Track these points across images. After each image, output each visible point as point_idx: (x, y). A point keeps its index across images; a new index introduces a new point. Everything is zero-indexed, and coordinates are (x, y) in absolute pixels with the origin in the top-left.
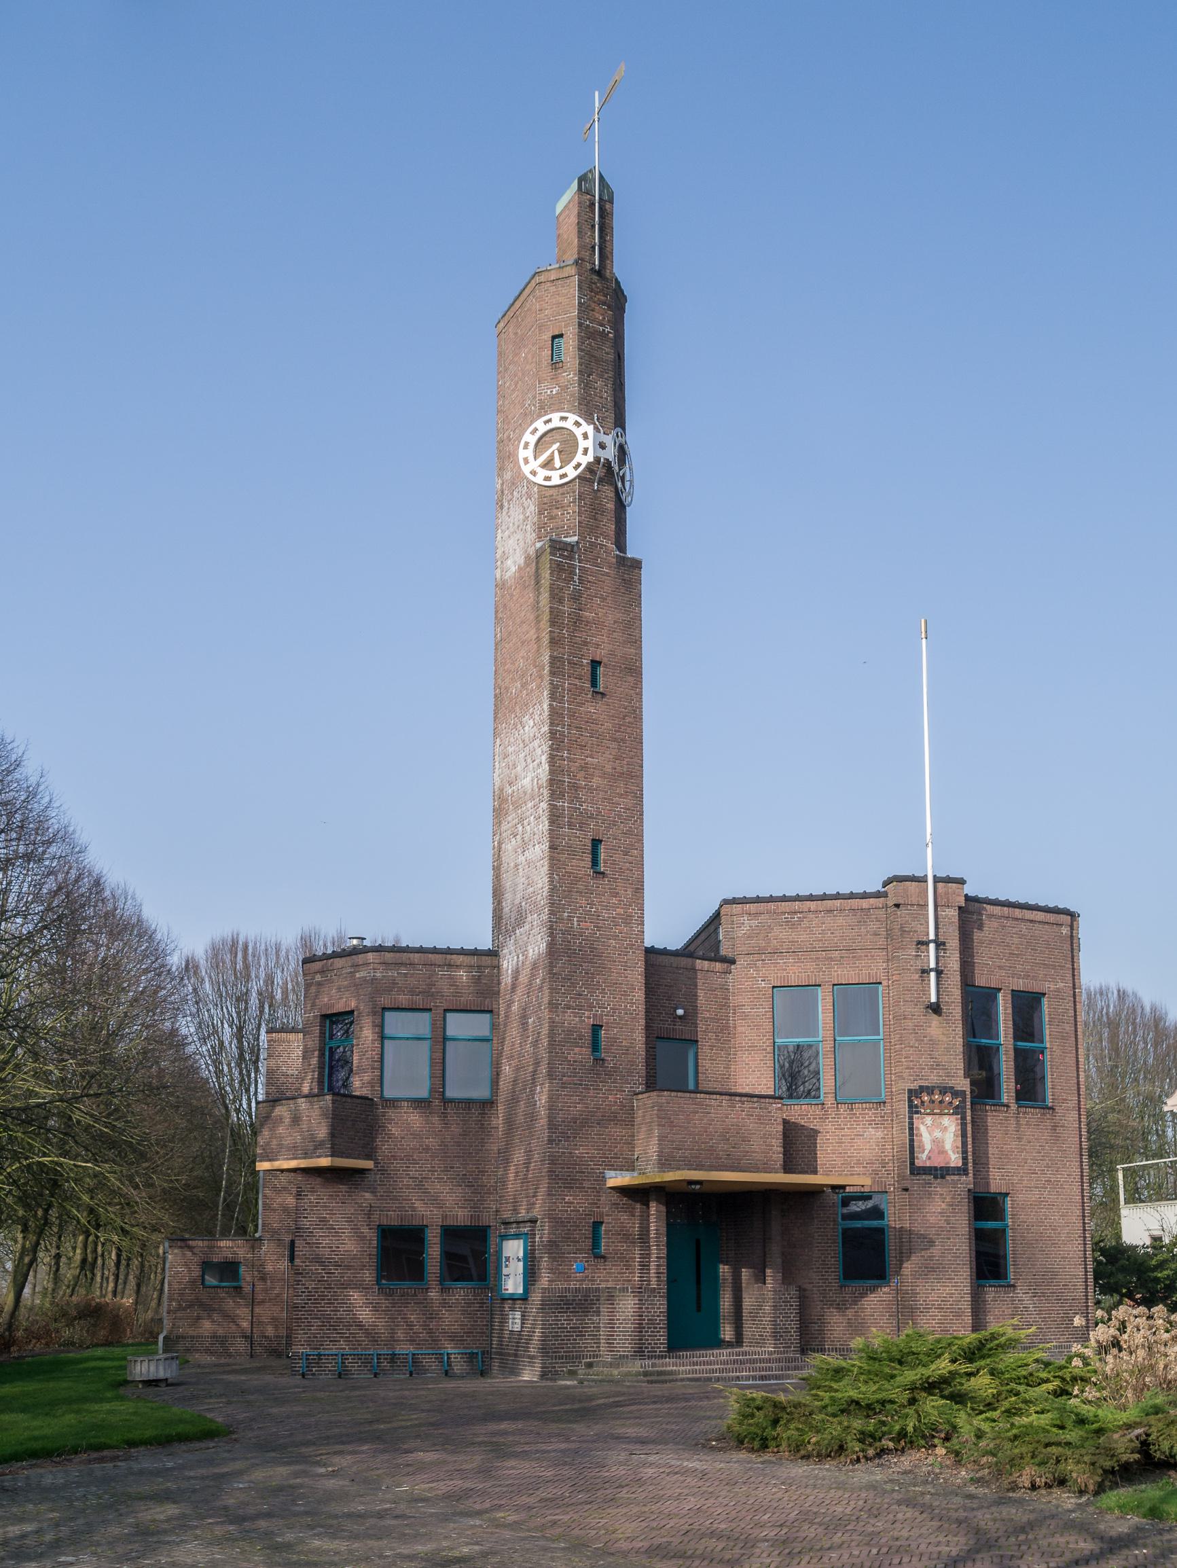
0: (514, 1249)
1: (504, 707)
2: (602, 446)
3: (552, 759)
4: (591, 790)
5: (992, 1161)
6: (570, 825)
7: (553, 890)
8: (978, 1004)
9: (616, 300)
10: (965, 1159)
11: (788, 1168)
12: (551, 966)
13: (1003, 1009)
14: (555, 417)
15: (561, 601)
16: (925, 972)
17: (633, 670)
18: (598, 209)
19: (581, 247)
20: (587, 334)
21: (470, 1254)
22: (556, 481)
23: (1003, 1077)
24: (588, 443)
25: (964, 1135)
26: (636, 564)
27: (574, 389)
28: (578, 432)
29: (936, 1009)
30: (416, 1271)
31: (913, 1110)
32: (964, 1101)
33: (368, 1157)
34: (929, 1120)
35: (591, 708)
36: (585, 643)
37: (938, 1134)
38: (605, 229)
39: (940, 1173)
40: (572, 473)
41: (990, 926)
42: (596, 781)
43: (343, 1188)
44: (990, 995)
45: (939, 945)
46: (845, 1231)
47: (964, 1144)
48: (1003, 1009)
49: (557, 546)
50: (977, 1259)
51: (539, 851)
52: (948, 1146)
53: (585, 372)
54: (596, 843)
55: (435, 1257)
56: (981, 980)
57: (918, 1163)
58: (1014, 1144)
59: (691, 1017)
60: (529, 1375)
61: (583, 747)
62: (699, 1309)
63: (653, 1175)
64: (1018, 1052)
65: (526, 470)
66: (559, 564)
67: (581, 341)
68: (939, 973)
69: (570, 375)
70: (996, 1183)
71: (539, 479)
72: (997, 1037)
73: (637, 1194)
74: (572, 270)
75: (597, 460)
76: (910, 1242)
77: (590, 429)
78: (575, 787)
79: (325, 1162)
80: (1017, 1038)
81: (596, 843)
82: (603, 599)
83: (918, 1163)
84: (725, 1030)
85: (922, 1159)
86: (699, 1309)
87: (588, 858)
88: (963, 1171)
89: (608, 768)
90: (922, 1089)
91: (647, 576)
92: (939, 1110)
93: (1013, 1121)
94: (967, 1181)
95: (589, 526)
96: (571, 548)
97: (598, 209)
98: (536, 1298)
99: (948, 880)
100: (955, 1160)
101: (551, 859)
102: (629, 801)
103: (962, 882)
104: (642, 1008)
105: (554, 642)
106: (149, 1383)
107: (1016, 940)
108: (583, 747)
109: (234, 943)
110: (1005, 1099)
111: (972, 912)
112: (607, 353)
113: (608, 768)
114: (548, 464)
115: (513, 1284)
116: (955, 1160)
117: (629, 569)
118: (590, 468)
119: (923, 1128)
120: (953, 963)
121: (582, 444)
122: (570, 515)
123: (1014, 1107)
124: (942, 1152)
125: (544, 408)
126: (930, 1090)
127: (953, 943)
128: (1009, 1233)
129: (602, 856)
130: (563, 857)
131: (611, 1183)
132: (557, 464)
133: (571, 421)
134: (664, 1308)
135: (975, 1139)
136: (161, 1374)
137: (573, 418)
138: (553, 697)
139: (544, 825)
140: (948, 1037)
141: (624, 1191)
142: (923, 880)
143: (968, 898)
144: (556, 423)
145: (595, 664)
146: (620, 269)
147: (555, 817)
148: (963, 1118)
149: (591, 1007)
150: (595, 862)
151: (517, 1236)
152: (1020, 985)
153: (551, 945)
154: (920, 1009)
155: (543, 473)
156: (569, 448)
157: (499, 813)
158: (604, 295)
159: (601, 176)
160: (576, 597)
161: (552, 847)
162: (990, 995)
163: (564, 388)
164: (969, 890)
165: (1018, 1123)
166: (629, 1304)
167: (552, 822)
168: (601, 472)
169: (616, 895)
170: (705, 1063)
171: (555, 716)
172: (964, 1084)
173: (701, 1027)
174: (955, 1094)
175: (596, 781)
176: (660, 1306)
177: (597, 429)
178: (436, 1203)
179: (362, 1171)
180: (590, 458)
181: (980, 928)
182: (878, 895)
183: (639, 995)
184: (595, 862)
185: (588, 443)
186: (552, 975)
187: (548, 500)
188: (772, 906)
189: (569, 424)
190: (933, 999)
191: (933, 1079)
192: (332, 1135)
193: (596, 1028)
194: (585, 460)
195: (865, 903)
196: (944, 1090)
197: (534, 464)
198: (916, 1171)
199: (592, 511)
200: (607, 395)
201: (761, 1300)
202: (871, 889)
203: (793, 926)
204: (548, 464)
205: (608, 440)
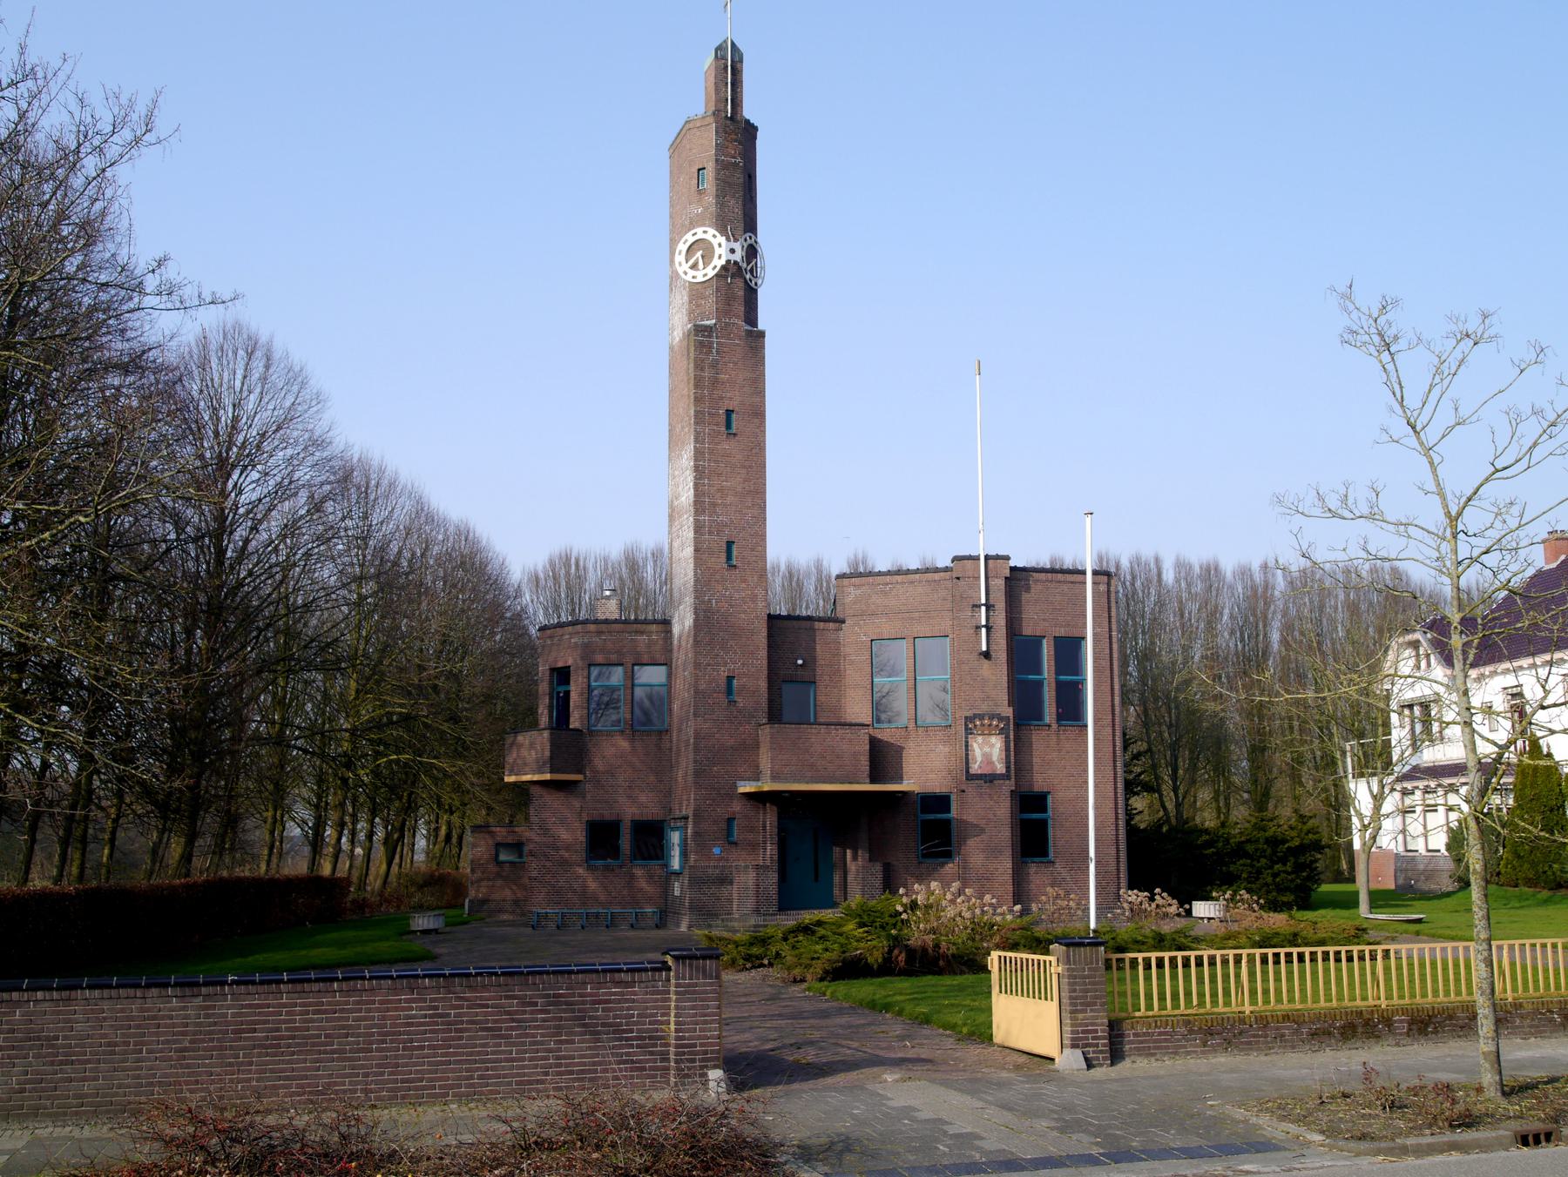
0: (675, 837)
1: (674, 443)
2: (733, 251)
3: (696, 485)
4: (725, 505)
5: (1035, 768)
6: (710, 533)
7: (697, 581)
8: (1022, 652)
9: (748, 133)
10: (1008, 768)
11: (873, 780)
12: (695, 636)
13: (1047, 650)
14: (699, 230)
15: (702, 370)
16: (978, 628)
17: (758, 414)
18: (729, 68)
19: (717, 101)
20: (721, 166)
21: (650, 838)
22: (700, 279)
23: (1046, 704)
24: (723, 249)
25: (1007, 749)
26: (762, 334)
27: (713, 209)
28: (715, 242)
29: (987, 655)
30: (615, 852)
31: (968, 731)
32: (1008, 724)
33: (579, 772)
34: (980, 739)
35: (726, 445)
36: (721, 398)
37: (987, 749)
38: (737, 84)
39: (990, 778)
40: (711, 273)
41: (1036, 589)
42: (730, 499)
43: (562, 794)
44: (1036, 642)
45: (989, 607)
46: (923, 822)
47: (1008, 756)
48: (1047, 650)
49: (699, 330)
50: (662, 847)
51: (689, 551)
52: (995, 758)
53: (721, 195)
54: (730, 544)
55: (625, 842)
56: (1027, 630)
57: (972, 771)
58: (1055, 754)
59: (810, 663)
60: (683, 928)
61: (719, 475)
62: (816, 879)
63: (767, 786)
64: (1060, 686)
65: (680, 271)
66: (701, 343)
67: (718, 172)
68: (988, 628)
69: (710, 199)
70: (1039, 783)
71: (689, 278)
72: (1039, 672)
73: (758, 798)
74: (711, 120)
75: (728, 262)
76: (968, 829)
77: (723, 240)
78: (714, 505)
79: (548, 777)
80: (1058, 672)
81: (730, 544)
82: (735, 364)
83: (972, 771)
84: (837, 674)
85: (975, 768)
86: (816, 879)
87: (723, 556)
88: (1006, 776)
89: (739, 489)
90: (975, 716)
91: (769, 341)
92: (987, 732)
93: (1054, 738)
94: (1010, 785)
95: (724, 311)
96: (709, 329)
97: (729, 68)
98: (686, 872)
99: (997, 557)
100: (1000, 768)
101: (696, 558)
102: (756, 512)
103: (1007, 558)
104: (765, 662)
105: (698, 400)
106: (425, 932)
107: (1058, 598)
108: (719, 475)
109: (568, 559)
110: (1047, 720)
111: (1018, 579)
112: (739, 178)
113: (739, 489)
114: (694, 267)
115: (676, 864)
116: (1000, 768)
117: (756, 339)
118: (724, 268)
119: (975, 745)
120: (1000, 620)
121: (718, 251)
122: (710, 304)
123: (1054, 726)
124: (990, 763)
125: (693, 225)
126: (981, 717)
127: (1000, 605)
128: (1050, 822)
129: (735, 553)
130: (705, 557)
131: (741, 790)
132: (701, 265)
133: (711, 234)
134: (775, 880)
135: (1018, 751)
136: (431, 927)
137: (712, 231)
138: (696, 440)
139: (691, 535)
140: (996, 676)
141: (749, 796)
142: (977, 558)
143: (1013, 569)
144: (700, 235)
145: (729, 413)
146: (749, 112)
147: (698, 529)
148: (1007, 737)
149: (726, 664)
150: (729, 557)
151: (677, 829)
152: (1062, 632)
153: (696, 620)
154: (975, 656)
155: (691, 273)
156: (708, 257)
157: (671, 518)
158: (738, 136)
159: (733, 44)
160: (714, 365)
161: (696, 550)
162: (1036, 642)
163: (706, 209)
164: (1012, 563)
165: (1059, 739)
166: (750, 876)
167: (696, 532)
168: (733, 269)
169: (745, 581)
170: (821, 698)
171: (698, 454)
172: (1008, 712)
173: (819, 672)
174: (1001, 719)
175: (730, 499)
176: (773, 878)
177: (728, 240)
178: (632, 806)
179: (576, 782)
180: (723, 262)
181: (1028, 590)
182: (946, 569)
183: (763, 653)
184: (729, 557)
185: (723, 249)
186: (696, 643)
187: (696, 291)
188: (871, 579)
189: (708, 237)
190: (984, 648)
191: (984, 708)
192: (551, 758)
193: (730, 679)
194: (719, 263)
195: (936, 576)
196: (992, 717)
197: (686, 267)
198: (970, 777)
199: (726, 300)
200: (738, 211)
201: (856, 873)
202: (940, 565)
203: (885, 593)
204: (694, 267)
205: (737, 246)
